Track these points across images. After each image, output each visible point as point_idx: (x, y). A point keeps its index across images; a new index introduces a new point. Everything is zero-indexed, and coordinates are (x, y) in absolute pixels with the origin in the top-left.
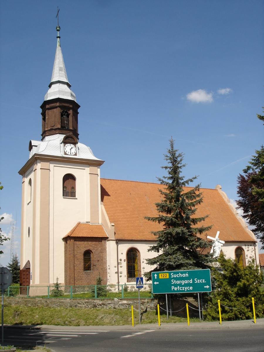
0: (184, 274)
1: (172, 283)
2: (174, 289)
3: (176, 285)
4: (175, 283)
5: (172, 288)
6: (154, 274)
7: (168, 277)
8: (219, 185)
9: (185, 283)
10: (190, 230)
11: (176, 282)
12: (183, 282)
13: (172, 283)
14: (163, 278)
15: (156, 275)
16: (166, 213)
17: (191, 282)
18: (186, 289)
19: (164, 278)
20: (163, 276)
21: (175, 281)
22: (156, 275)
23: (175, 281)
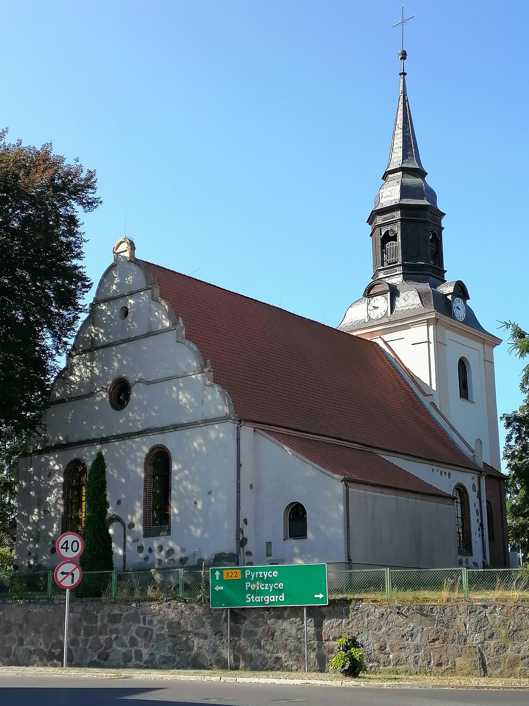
0: (273, 597)
1: (247, 601)
2: (249, 588)
3: (256, 593)
4: (253, 601)
5: (247, 586)
6: (214, 571)
7: (239, 577)
8: (100, 642)
9: (272, 600)
10: (49, 342)
11: (254, 599)
12: (266, 599)
13: (247, 601)
14: (229, 578)
15: (217, 573)
16: (75, 262)
17: (281, 598)
18: (266, 576)
19: (232, 578)
20: (230, 575)
21: (253, 597)
22: (217, 573)
23: (253, 597)
